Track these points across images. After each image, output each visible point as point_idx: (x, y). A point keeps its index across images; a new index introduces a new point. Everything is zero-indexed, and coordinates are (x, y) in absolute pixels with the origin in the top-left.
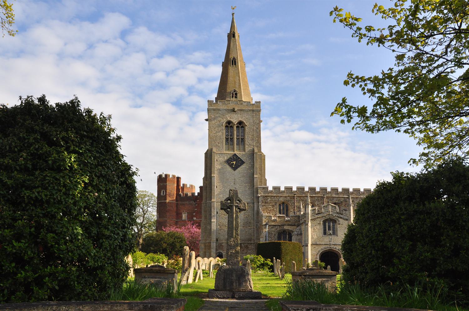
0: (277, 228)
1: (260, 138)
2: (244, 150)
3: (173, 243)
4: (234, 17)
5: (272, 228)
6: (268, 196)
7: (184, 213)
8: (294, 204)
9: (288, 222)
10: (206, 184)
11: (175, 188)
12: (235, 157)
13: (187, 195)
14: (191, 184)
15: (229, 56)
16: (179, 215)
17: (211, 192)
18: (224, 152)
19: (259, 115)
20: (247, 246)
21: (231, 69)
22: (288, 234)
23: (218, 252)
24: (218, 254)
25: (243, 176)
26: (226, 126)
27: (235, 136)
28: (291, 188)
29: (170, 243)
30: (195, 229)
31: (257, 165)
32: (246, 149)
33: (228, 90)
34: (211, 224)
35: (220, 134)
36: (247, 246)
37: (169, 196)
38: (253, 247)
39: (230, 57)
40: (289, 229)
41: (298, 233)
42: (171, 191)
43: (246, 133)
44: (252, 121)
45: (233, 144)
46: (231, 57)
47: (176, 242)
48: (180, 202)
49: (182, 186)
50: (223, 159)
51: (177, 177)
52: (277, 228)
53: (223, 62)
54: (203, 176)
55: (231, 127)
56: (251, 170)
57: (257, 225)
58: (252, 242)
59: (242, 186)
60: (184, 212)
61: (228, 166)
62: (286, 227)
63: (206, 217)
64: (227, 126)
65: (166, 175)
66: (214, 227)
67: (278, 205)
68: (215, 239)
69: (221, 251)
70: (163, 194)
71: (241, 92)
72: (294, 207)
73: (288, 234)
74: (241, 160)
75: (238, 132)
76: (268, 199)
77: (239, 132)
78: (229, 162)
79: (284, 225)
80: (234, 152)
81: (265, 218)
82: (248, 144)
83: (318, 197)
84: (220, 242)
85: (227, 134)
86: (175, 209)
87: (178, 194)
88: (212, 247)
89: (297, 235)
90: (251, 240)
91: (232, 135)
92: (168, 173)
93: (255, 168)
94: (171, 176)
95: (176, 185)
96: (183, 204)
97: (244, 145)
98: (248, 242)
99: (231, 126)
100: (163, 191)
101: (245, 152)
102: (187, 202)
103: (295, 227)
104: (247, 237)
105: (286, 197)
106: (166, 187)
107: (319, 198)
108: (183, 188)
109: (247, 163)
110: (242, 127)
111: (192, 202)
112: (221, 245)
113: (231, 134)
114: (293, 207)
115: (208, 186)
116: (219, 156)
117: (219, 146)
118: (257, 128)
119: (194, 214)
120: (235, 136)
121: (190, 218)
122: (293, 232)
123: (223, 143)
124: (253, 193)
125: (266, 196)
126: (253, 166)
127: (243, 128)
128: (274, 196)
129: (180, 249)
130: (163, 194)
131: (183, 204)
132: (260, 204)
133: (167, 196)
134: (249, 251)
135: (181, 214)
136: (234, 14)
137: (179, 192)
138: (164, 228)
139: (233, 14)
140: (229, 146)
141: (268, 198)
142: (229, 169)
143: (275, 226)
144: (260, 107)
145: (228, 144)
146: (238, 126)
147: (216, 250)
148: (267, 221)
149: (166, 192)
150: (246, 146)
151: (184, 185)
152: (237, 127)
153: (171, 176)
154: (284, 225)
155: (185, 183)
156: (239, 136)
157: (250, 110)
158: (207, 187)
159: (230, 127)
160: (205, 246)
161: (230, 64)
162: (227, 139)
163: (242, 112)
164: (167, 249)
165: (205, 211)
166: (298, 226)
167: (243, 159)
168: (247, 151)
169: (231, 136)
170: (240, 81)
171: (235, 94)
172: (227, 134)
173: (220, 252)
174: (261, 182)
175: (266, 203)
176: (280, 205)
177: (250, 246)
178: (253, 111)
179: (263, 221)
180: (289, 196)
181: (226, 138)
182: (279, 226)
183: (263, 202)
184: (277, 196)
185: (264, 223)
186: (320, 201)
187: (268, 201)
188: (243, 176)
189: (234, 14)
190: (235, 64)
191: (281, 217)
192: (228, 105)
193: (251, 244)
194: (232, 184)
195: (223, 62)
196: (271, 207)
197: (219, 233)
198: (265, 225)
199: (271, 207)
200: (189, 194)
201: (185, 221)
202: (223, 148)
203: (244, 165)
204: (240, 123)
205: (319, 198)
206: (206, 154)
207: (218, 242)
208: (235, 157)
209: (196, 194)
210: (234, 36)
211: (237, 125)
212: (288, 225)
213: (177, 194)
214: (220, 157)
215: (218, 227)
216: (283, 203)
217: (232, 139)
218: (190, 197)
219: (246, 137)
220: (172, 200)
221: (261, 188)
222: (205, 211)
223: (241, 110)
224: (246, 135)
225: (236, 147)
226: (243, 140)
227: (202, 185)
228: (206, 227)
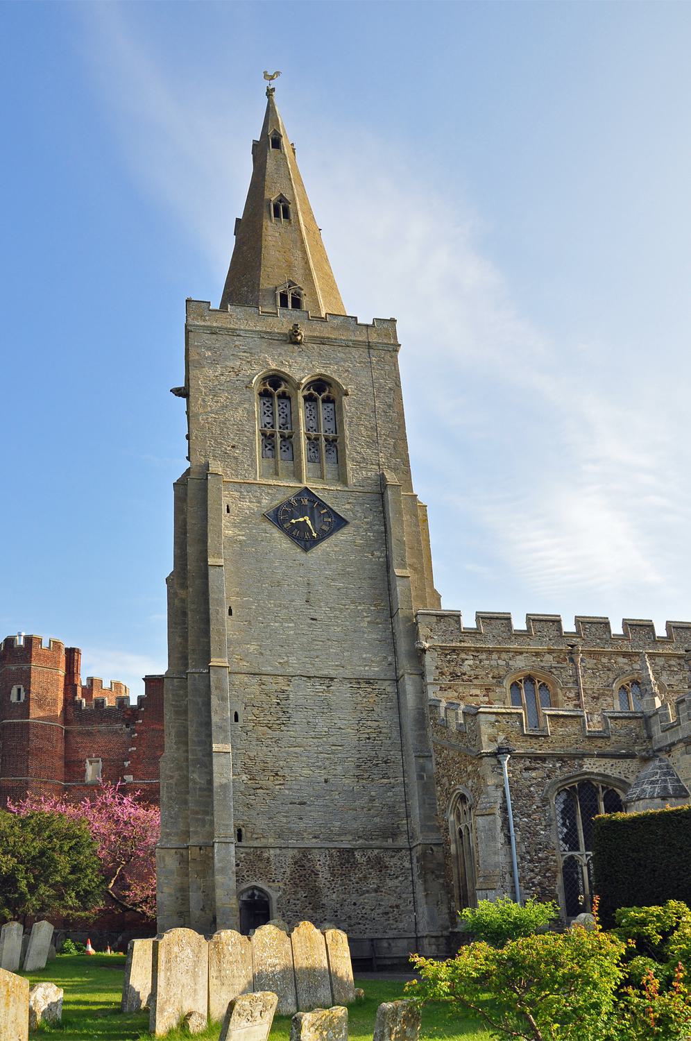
0: (552, 771)
1: (404, 440)
2: (342, 478)
3: (42, 853)
4: (275, 100)
5: (527, 769)
6: (464, 650)
7: (91, 763)
8: (576, 682)
9: (599, 743)
10: (183, 601)
11: (58, 680)
12: (305, 502)
13: (100, 703)
14: (115, 680)
15: (263, 194)
16: (73, 768)
17: (206, 632)
18: (259, 480)
19: (395, 364)
20: (379, 860)
21: (272, 230)
22: (602, 795)
23: (245, 886)
24: (244, 898)
25: (344, 574)
26: (264, 394)
27: (303, 429)
28: (553, 621)
29: (29, 853)
30: (129, 809)
31: (400, 531)
32: (350, 474)
33: (265, 284)
34: (209, 765)
35: (240, 414)
36: (379, 860)
37: (40, 707)
38: (407, 865)
39: (267, 195)
40: (608, 772)
41: (665, 788)
42: (47, 690)
43: (346, 421)
44: (365, 381)
45: (294, 457)
46: (272, 196)
47: (53, 849)
48: (76, 728)
49: (84, 683)
50: (254, 506)
51: (66, 649)
52: (552, 771)
53: (238, 220)
54: (169, 568)
55: (283, 396)
56: (377, 553)
57: (422, 769)
58: (402, 841)
59: (341, 611)
60: (89, 757)
61: (276, 534)
62: (592, 766)
63: (183, 736)
64: (266, 391)
65: (29, 640)
66: (224, 771)
67: (507, 684)
68: (232, 830)
69: (260, 884)
70: (19, 698)
71: (314, 293)
72: (578, 696)
73: (602, 795)
74: (332, 513)
75: (313, 416)
76: (463, 660)
77: (317, 418)
78: (279, 517)
79: (583, 756)
80: (301, 482)
81: (493, 725)
82: (358, 457)
83: (668, 656)
84: (256, 844)
85: (268, 420)
86: (60, 747)
87: (69, 701)
88: (217, 865)
89: (664, 798)
90: (394, 835)
91: (290, 421)
92: (35, 633)
93: (393, 541)
94: (45, 644)
95: (62, 672)
96: (89, 734)
97: (340, 462)
98: (385, 844)
99: (284, 393)
100: (19, 690)
101: (345, 483)
102: (102, 727)
103: (633, 764)
104: (377, 820)
105: (537, 654)
106: (30, 677)
107: (672, 662)
108: (88, 691)
109: (358, 527)
110: (327, 400)
111: (118, 726)
112: (260, 858)
113: (282, 421)
114: (572, 695)
115: (191, 607)
116: (237, 494)
117: (236, 458)
118: (390, 406)
119: (127, 764)
120: (303, 429)
121: (113, 772)
122: (625, 785)
123: (252, 450)
124: (392, 643)
125: (454, 650)
126: (385, 537)
127: (331, 406)
128: (490, 652)
129: (71, 877)
130: (19, 698)
131: (89, 734)
132: (430, 679)
133: (33, 705)
134: (390, 883)
135: (82, 762)
136: (273, 90)
137: (76, 694)
138: (13, 803)
139: (270, 93)
140: (276, 463)
141: (463, 656)
142: (280, 542)
143: (543, 758)
144: (396, 338)
145: (274, 457)
146: (311, 395)
147: (240, 879)
148: (501, 738)
149: (28, 692)
150: (350, 465)
151: (91, 680)
152: (308, 399)
153: (45, 644)
154: (583, 756)
155: (95, 675)
156: (317, 430)
157: (356, 344)
158: (185, 614)
159: (279, 397)
160: (184, 861)
161: (266, 214)
162: (268, 438)
163: (326, 347)
164: (19, 877)
165: (177, 713)
166: (646, 760)
167: (342, 509)
168: (352, 480)
169: (283, 426)
170: (307, 262)
171: (292, 300)
172: (268, 420)
173: (255, 888)
174: (422, 599)
175: (454, 676)
176: (515, 686)
177: (394, 860)
178: (369, 346)
179: (485, 738)
180: (550, 652)
181: (264, 434)
182: (560, 758)
183: (442, 674)
184: (499, 651)
185: (487, 748)
186: (676, 673)
187: (465, 668)
188: (344, 574)
189: (273, 90)
190: (286, 216)
191: (567, 721)
192: (270, 319)
193: (399, 850)
194: (299, 602)
195: (238, 220)
196: (477, 692)
197: (249, 806)
198: (494, 755)
199: (477, 692)
200: (110, 702)
201: (95, 786)
202: (253, 464)
203: (345, 530)
204: (320, 384)
205: (672, 662)
206: (181, 486)
207: (243, 843)
208: (308, 501)
209: (134, 702)
210: (277, 144)
211: (306, 393)
212: (602, 756)
213: (65, 700)
214: (242, 498)
215: (244, 777)
216: (530, 679)
217: (289, 440)
218: (111, 709)
219: (347, 433)
220: (50, 719)
221: (428, 619)
222: (182, 712)
223: (322, 341)
224: (346, 427)
225: (309, 470)
226: (334, 444)
227: (241, 217)
228: (185, 780)
